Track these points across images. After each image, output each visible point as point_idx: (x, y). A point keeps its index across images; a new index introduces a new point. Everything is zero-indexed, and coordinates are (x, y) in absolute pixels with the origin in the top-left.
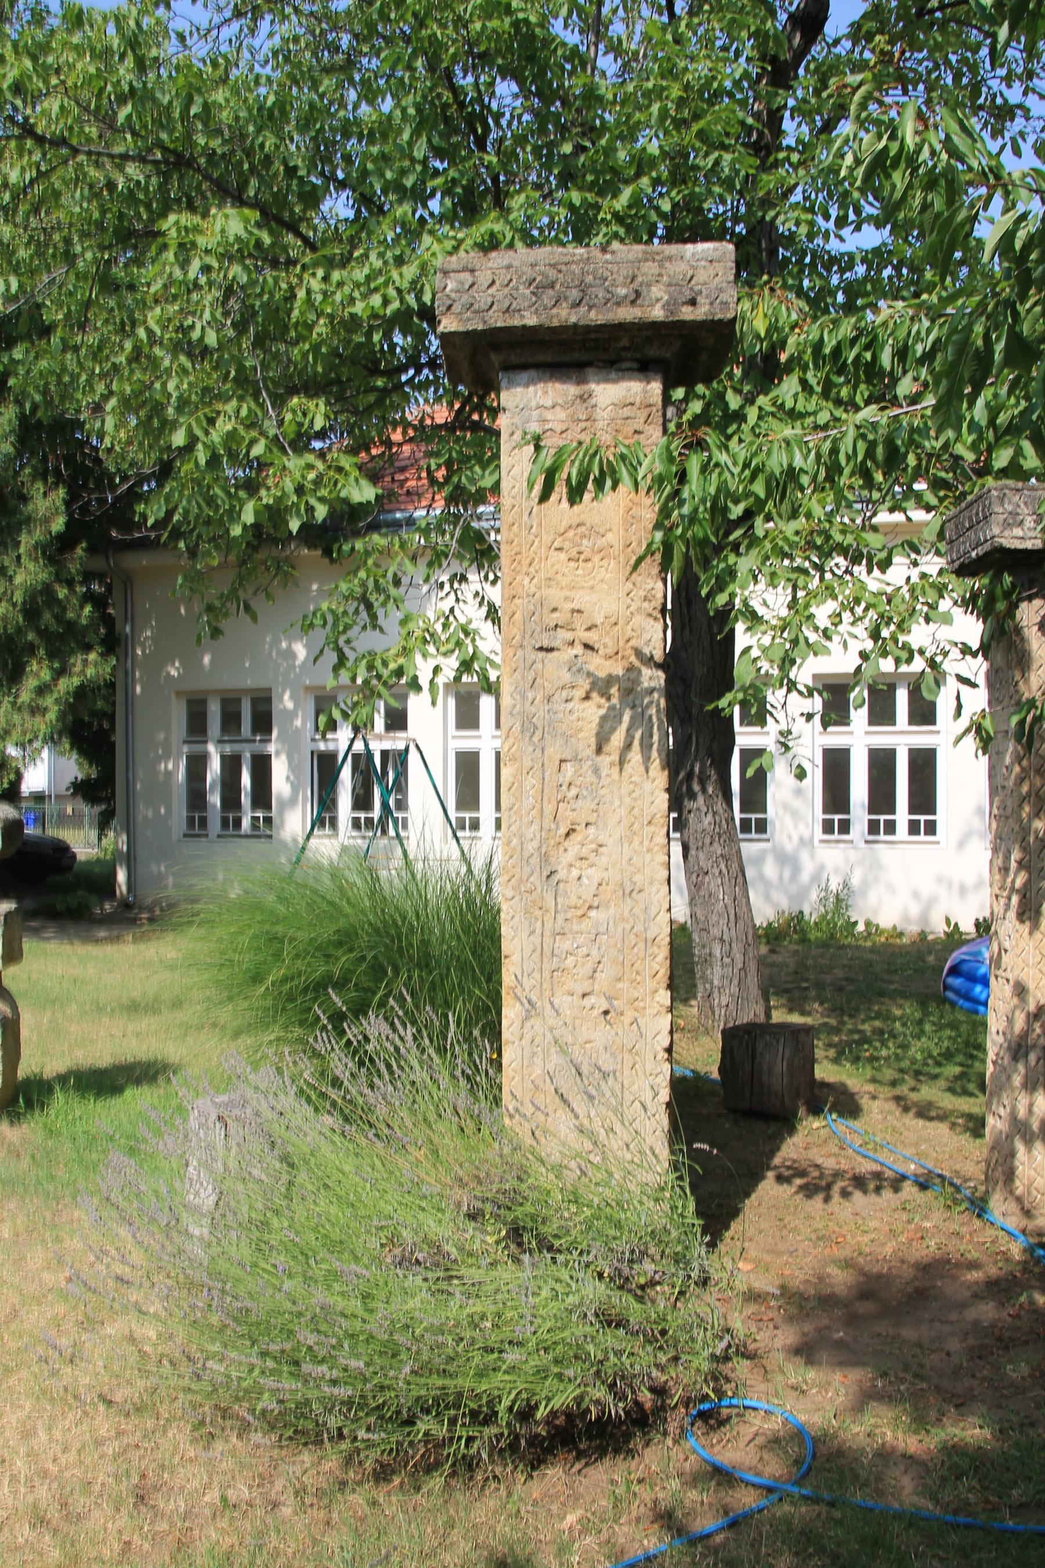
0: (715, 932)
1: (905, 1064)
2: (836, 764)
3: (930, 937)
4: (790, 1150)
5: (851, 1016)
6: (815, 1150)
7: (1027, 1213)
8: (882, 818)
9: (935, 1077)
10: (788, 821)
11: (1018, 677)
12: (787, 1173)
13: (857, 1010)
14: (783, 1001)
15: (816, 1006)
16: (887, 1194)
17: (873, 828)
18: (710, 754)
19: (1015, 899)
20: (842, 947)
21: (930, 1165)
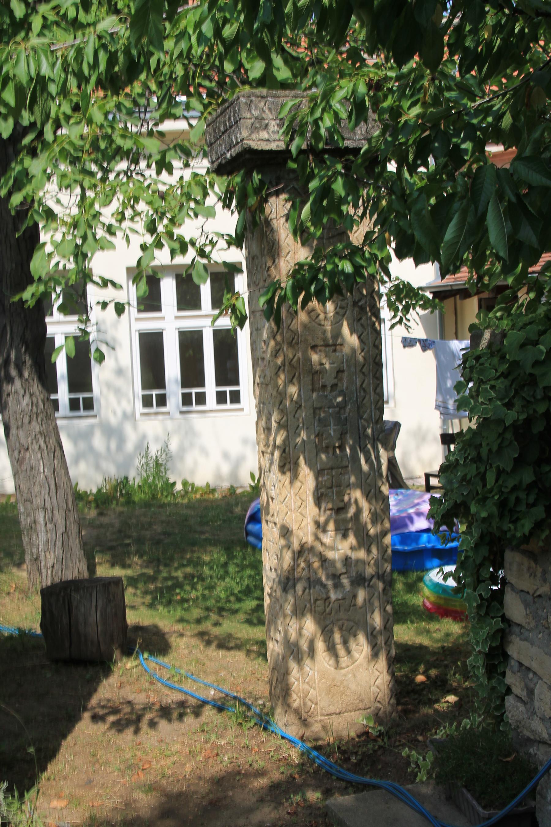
0: (38, 501)
1: (211, 603)
2: (151, 345)
3: (239, 491)
4: (107, 690)
5: (166, 565)
6: (128, 688)
7: (305, 723)
8: (194, 391)
9: (235, 612)
10: (112, 398)
11: (269, 263)
12: (101, 712)
13: (172, 559)
14: (108, 557)
15: (136, 559)
16: (189, 720)
17: (186, 400)
18: (24, 341)
19: (277, 454)
20: (162, 506)
21: (227, 689)
